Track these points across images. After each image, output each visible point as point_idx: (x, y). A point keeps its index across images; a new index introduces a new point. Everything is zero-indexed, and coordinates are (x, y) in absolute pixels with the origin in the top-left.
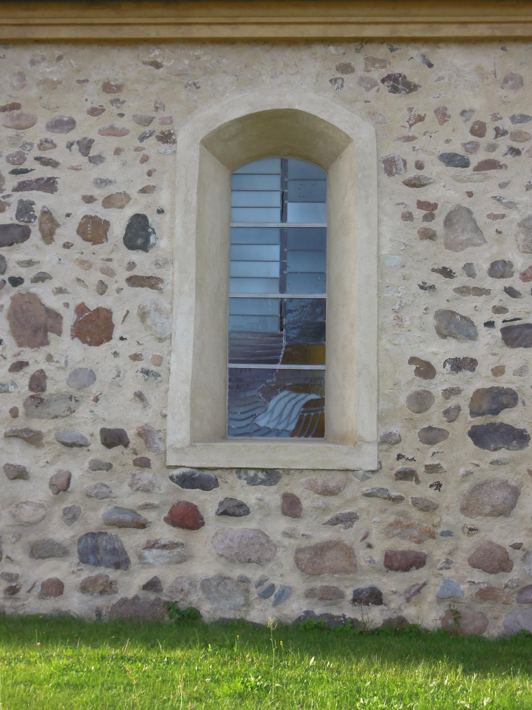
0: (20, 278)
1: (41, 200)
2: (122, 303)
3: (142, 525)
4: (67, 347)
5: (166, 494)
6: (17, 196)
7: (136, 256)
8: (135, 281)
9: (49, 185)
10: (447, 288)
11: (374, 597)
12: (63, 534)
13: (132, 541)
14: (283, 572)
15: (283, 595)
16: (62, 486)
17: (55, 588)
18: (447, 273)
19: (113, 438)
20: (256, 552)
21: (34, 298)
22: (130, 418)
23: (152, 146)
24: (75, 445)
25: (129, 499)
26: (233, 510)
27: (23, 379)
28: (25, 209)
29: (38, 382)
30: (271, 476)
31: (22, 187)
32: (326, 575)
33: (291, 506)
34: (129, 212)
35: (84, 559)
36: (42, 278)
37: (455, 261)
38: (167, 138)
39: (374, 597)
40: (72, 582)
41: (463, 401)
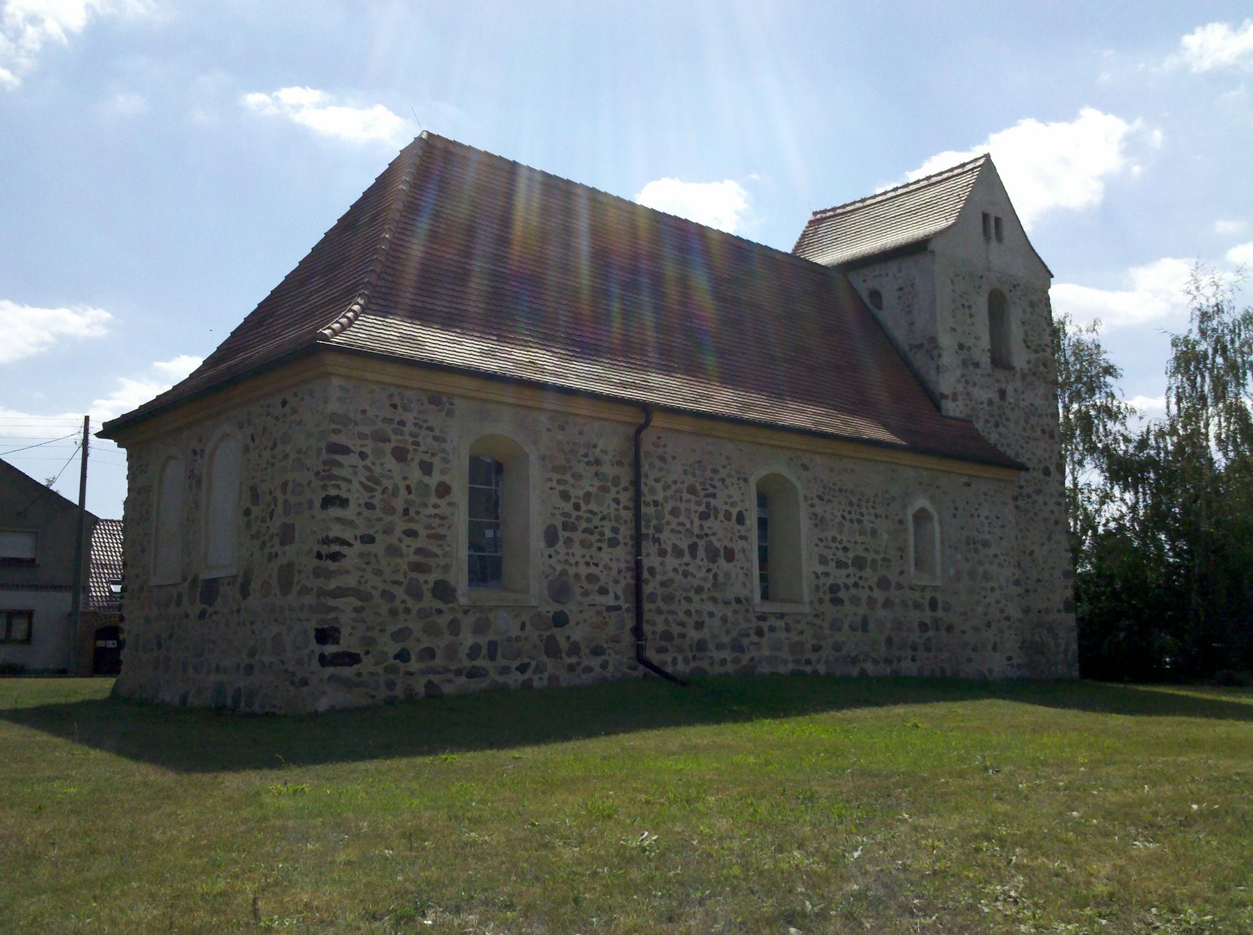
0: (549, 527)
1: (713, 502)
2: (737, 546)
3: (748, 635)
4: (722, 562)
5: (755, 623)
6: (705, 500)
7: (740, 527)
8: (741, 537)
9: (714, 496)
10: (822, 545)
11: (808, 662)
12: (726, 639)
13: (745, 641)
14: (785, 654)
15: (786, 662)
16: (724, 620)
17: (723, 662)
18: (821, 540)
19: (738, 601)
20: (777, 647)
21: (711, 542)
22: (743, 593)
23: (742, 483)
24: (727, 603)
25: (744, 625)
26: (772, 629)
27: (710, 576)
28: (708, 505)
29: (715, 576)
30: (782, 616)
31: (706, 496)
32: (453, 668)
33: (788, 629)
34: (738, 509)
35: (732, 649)
36: (714, 534)
37: (823, 537)
38: (746, 480)
39: (808, 662)
40: (729, 659)
41: (826, 588)
